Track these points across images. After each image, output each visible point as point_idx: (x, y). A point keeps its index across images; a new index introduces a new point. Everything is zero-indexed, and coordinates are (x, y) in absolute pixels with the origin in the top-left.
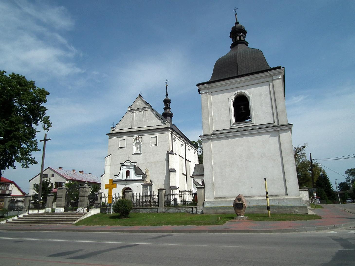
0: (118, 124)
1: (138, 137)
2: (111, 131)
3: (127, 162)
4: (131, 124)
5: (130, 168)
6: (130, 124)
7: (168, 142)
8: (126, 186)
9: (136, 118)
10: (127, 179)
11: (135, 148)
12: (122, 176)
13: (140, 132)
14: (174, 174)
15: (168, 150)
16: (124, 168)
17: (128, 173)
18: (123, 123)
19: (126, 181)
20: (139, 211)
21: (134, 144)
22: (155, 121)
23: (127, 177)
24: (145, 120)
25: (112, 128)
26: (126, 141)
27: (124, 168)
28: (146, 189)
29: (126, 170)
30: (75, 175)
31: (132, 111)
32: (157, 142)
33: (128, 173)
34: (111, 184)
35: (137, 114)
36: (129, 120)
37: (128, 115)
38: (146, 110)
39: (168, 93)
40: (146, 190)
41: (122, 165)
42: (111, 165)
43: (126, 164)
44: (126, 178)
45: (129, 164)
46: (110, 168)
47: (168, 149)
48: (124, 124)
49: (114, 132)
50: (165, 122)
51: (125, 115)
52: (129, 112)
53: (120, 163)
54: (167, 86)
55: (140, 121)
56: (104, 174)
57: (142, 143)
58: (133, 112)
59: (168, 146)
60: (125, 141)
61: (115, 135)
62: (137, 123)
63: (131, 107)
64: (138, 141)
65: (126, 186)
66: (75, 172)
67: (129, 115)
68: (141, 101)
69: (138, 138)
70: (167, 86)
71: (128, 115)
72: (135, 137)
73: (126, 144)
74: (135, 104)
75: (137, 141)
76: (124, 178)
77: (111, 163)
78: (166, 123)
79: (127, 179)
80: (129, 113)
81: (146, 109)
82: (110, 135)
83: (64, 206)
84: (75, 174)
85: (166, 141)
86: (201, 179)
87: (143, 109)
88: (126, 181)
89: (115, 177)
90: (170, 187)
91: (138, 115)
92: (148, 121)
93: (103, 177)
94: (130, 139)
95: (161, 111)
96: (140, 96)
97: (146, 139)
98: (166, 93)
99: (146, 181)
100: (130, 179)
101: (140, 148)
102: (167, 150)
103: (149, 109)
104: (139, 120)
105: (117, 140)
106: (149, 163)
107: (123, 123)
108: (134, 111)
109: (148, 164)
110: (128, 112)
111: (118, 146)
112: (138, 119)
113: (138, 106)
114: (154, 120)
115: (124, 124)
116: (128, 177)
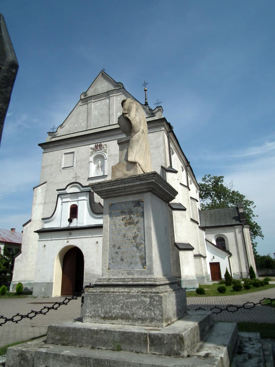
0: (61, 126)
1: (99, 144)
2: (48, 139)
3: (72, 187)
4: (85, 124)
5: (80, 198)
6: (83, 124)
7: (162, 149)
8: (68, 242)
9: (95, 113)
10: (70, 226)
11: (93, 167)
12: (61, 220)
13: (102, 135)
14: (180, 213)
15: (164, 166)
16: (64, 200)
17: (74, 211)
18: (71, 123)
19: (69, 230)
20: (104, 294)
21: (91, 159)
23: (70, 221)
24: (113, 113)
25: (50, 133)
26: (75, 154)
27: (64, 200)
28: (130, 223)
29: (70, 205)
30: (13, 235)
31: (88, 101)
33: (74, 211)
34: (137, 274)
35: (98, 104)
36: (83, 116)
38: (115, 95)
39: (147, 98)
40: (131, 232)
41: (61, 194)
42: (45, 203)
43: (69, 190)
44: (68, 223)
45: (77, 190)
46: (44, 209)
47: (164, 162)
48: (72, 125)
49: (53, 140)
50: (154, 112)
51: (75, 109)
52: (82, 103)
54: (145, 90)
55: (103, 116)
56: (30, 221)
57: (106, 156)
58: (89, 102)
59: (163, 157)
60: (73, 154)
61: (55, 144)
62: (98, 120)
63: (85, 94)
64: (98, 151)
65: (68, 242)
66: (15, 232)
67: (83, 109)
68: (105, 81)
69: (99, 147)
70: (146, 90)
71: (81, 109)
72: (93, 146)
73: (75, 160)
75: (98, 153)
76: (65, 224)
77: (45, 199)
78: (157, 112)
79: (73, 225)
80: (83, 104)
81: (115, 93)
82: (45, 146)
84: (13, 234)
85: (158, 147)
86: (215, 234)
87: (108, 94)
88: (69, 230)
89: (45, 223)
90: (176, 245)
91: (99, 105)
93: (27, 227)
95: (144, 103)
96: (103, 74)
98: (146, 101)
99: (130, 159)
100: (80, 225)
101: (102, 167)
102: (160, 165)
103: (121, 93)
104: (101, 115)
105: (59, 156)
107: (71, 123)
108: (91, 99)
110: (80, 103)
111: (61, 165)
112: (99, 112)
113: (99, 91)
115: (72, 125)
116: (75, 220)
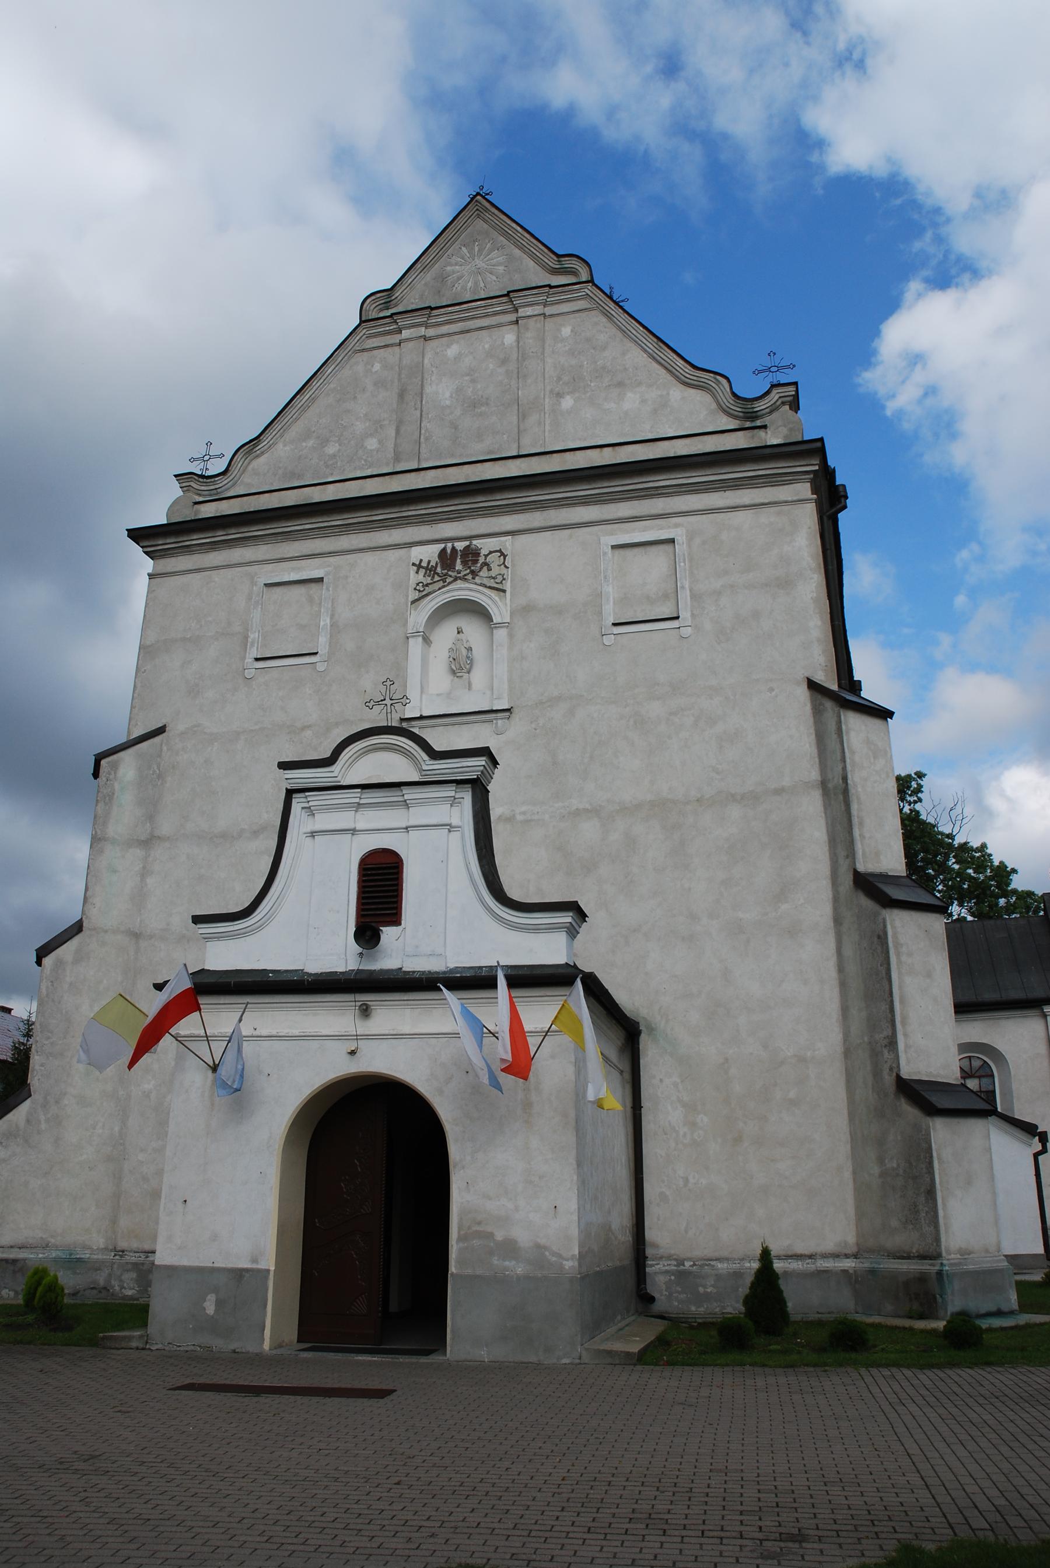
5: (418, 815)
17: (381, 888)
22: (643, 401)
23: (367, 935)
27: (323, 821)
32: (685, 596)
33: (381, 888)
37: (360, 368)
44: (354, 948)
48: (311, 443)
49: (209, 511)
53: (197, 920)
71: (360, 368)
74: (429, 276)
75: (461, 590)
76: (336, 951)
83: (815, 775)
91: (458, 358)
92: (567, 402)
93: (60, 963)
94: (379, 569)
97: (546, 558)
106: (594, 812)
107: (307, 435)
109: (589, 830)
112: (459, 390)
114: (629, 395)
116: (388, 933)
